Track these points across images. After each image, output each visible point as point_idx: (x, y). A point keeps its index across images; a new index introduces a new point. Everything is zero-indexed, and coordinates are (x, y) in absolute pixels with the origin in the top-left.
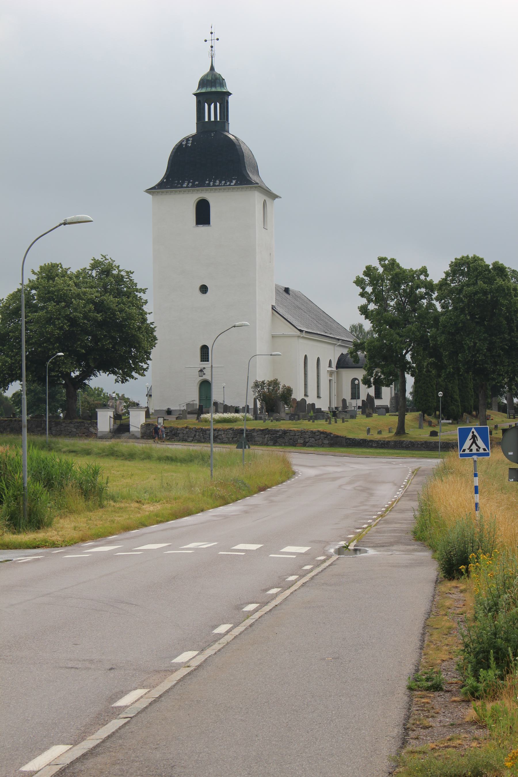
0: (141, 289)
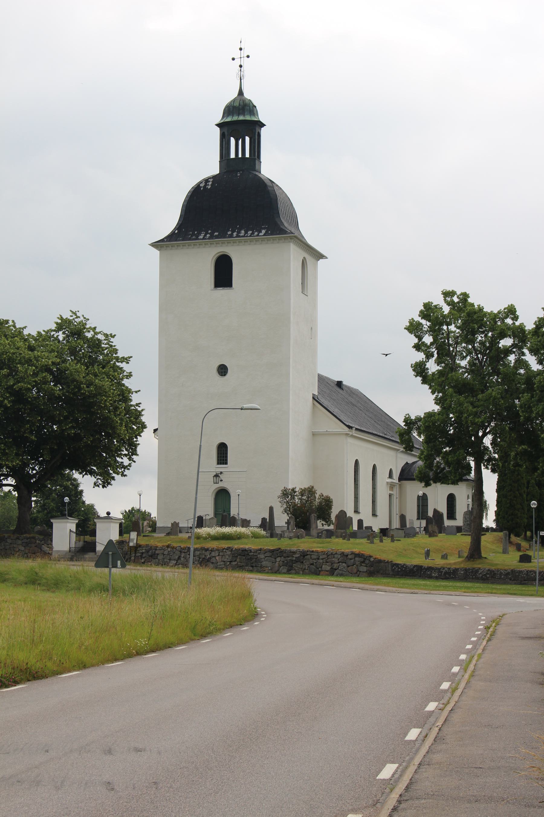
0: (123, 358)
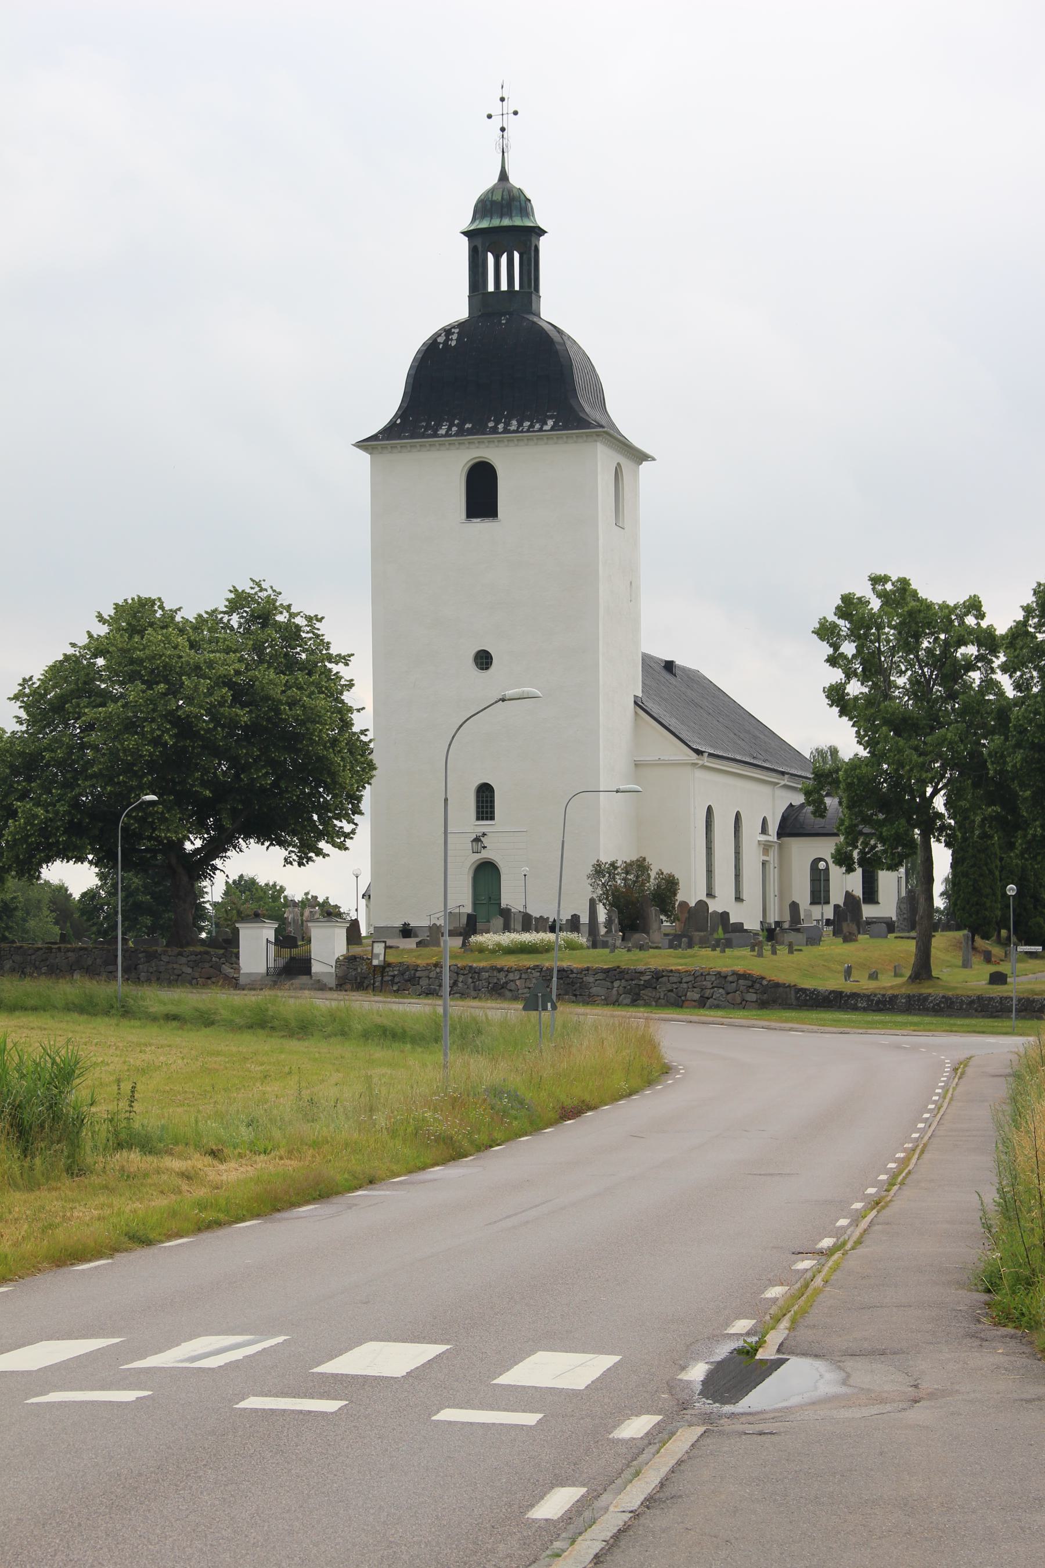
0: (339, 655)
